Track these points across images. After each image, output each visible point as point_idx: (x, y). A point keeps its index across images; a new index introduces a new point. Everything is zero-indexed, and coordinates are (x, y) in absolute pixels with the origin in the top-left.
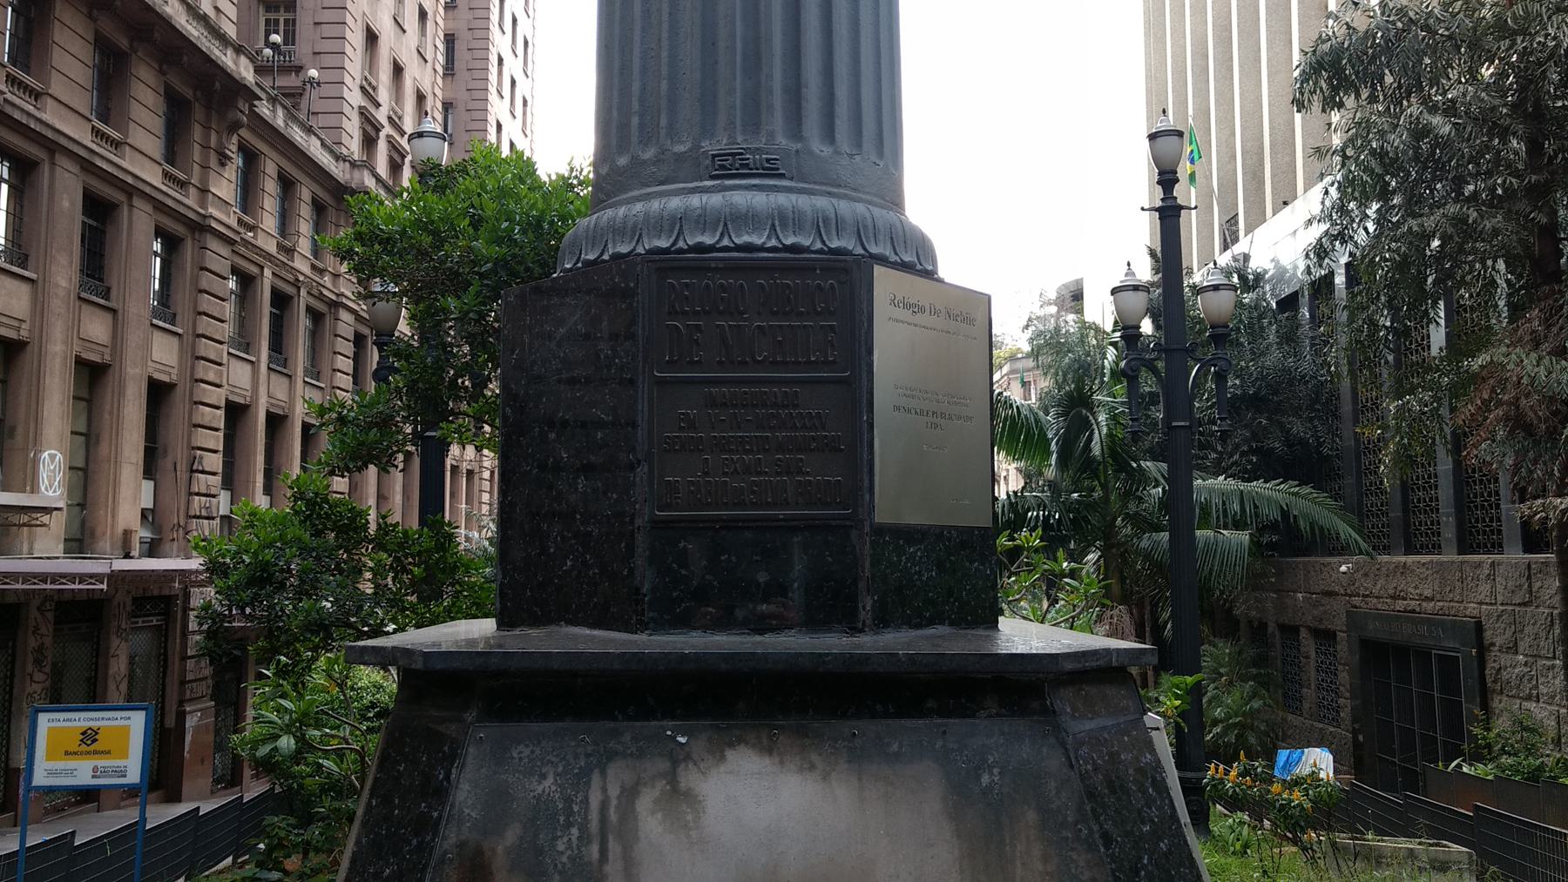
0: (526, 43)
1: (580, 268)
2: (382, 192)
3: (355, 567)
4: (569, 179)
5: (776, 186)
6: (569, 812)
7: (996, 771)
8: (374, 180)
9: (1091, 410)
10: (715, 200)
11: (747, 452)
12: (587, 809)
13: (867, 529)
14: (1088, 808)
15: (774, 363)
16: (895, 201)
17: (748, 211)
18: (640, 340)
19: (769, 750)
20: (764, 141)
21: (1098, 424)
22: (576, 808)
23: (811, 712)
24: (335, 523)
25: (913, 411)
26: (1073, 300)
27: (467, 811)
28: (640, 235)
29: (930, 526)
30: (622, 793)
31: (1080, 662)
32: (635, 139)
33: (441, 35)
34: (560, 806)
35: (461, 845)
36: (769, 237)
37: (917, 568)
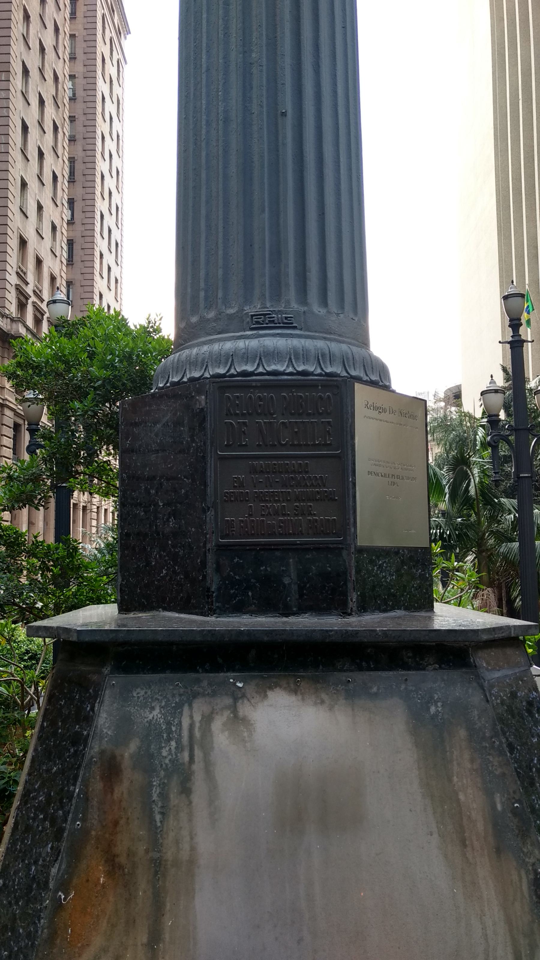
0: (117, 244)
1: (169, 387)
2: (29, 336)
3: (18, 568)
4: (148, 328)
5: (291, 334)
6: (170, 731)
7: (439, 704)
8: (25, 329)
9: (469, 467)
10: (253, 343)
11: (276, 501)
12: (181, 729)
13: (353, 550)
14: (499, 728)
15: (293, 445)
16: (365, 343)
17: (274, 350)
18: (209, 432)
19: (295, 692)
20: (283, 306)
21: (473, 475)
22: (174, 729)
23: (321, 667)
24: (5, 541)
25: (380, 475)
26: (455, 399)
27: (105, 731)
28: (207, 366)
29: (392, 547)
30: (202, 719)
31: (492, 635)
32: (202, 305)
33: (65, 240)
34: (164, 727)
35: (102, 752)
36: (288, 366)
37: (384, 574)
